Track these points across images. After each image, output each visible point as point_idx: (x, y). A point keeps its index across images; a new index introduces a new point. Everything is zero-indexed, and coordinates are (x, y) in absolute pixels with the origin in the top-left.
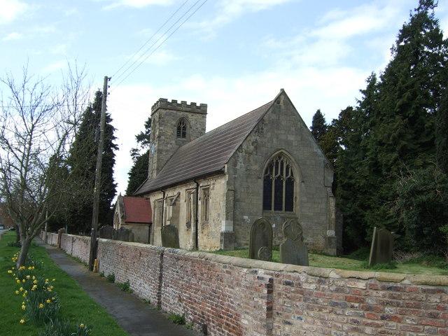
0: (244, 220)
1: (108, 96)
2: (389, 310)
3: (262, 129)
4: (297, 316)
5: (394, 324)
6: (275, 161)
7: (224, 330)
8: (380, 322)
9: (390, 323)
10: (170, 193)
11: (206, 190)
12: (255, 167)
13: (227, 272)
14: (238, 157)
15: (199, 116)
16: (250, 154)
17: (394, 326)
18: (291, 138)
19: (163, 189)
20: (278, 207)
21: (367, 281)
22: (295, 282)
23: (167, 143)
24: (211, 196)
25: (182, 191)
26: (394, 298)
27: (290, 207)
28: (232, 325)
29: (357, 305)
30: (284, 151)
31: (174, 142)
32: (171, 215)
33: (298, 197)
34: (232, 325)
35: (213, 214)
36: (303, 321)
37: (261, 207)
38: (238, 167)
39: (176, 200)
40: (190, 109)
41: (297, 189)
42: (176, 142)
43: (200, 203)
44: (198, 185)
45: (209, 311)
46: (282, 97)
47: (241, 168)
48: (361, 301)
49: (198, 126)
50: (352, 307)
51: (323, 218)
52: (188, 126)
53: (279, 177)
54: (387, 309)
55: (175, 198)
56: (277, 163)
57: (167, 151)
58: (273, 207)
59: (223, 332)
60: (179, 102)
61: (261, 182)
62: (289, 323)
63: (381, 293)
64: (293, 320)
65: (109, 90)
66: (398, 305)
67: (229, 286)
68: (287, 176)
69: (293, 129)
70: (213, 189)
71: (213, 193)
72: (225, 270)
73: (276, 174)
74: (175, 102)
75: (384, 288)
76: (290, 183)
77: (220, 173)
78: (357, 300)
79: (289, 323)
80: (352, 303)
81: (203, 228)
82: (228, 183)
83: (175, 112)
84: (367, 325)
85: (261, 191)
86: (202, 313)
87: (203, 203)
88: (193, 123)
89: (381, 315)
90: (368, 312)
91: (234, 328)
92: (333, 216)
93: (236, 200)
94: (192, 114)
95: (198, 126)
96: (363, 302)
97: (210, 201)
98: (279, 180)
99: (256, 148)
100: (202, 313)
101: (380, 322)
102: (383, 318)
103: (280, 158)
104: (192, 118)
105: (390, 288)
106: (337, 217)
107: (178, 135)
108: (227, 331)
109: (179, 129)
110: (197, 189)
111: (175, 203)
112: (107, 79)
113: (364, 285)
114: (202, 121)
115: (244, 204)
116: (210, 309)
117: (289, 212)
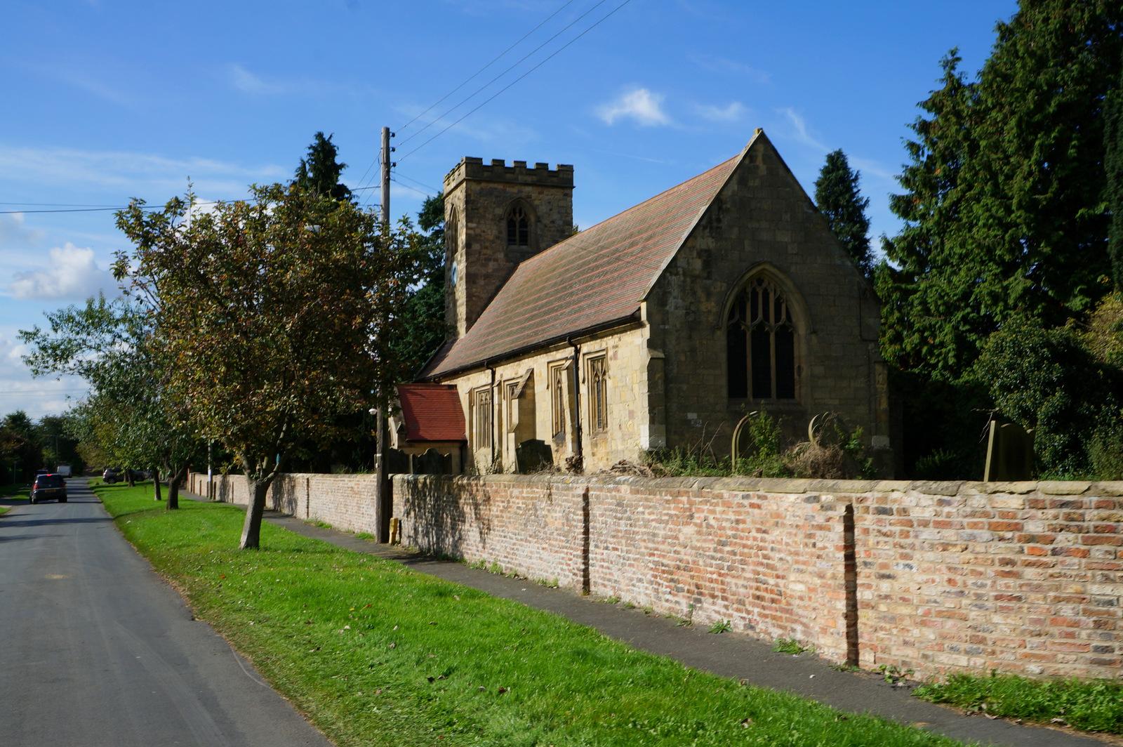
0: (688, 422)
1: (392, 169)
2: (1063, 540)
3: (719, 220)
4: (902, 562)
5: (1076, 560)
6: (749, 290)
7: (750, 608)
8: (1049, 559)
9: (1068, 560)
10: (506, 372)
11: (598, 361)
12: (708, 306)
13: (752, 505)
14: (669, 283)
15: (558, 193)
16: (695, 278)
17: (1074, 564)
18: (783, 237)
19: (492, 363)
20: (761, 391)
21: (1024, 496)
22: (895, 507)
23: (488, 260)
24: (610, 373)
25: (539, 364)
26: (1073, 520)
27: (787, 390)
28: (768, 596)
29: (1009, 535)
30: (767, 267)
31: (501, 256)
32: (515, 420)
33: (803, 365)
34: (768, 596)
35: (616, 413)
36: (914, 570)
37: (724, 392)
38: (670, 306)
39: (525, 387)
40: (535, 178)
41: (801, 349)
42: (506, 255)
43: (583, 389)
44: (577, 351)
45: (711, 581)
46: (761, 147)
47: (676, 308)
48: (1017, 527)
49: (555, 216)
50: (1001, 539)
51: (862, 410)
52: (532, 218)
53: (761, 327)
54: (1061, 537)
55: (522, 381)
56: (755, 294)
57: (487, 276)
58: (750, 392)
59: (748, 612)
60: (509, 163)
61: (721, 338)
62: (889, 577)
63: (1051, 512)
64: (898, 569)
65: (394, 157)
66: (1080, 530)
67: (759, 530)
68: (777, 319)
69: (787, 217)
70: (615, 356)
71: (613, 367)
72: (746, 502)
73: (754, 317)
74: (499, 163)
75: (1054, 505)
76: (786, 335)
77: (632, 322)
78: (1009, 527)
79: (889, 577)
80: (1001, 533)
81: (595, 445)
82: (651, 344)
83: (500, 187)
84: (1029, 564)
85: (723, 357)
86: (698, 586)
87: (591, 390)
88: (543, 209)
89: (1051, 547)
90: (1031, 545)
91: (773, 601)
92: (884, 405)
93: (667, 380)
94: (540, 189)
95: (555, 216)
96: (1018, 530)
97: (609, 383)
98: (760, 334)
99: (707, 264)
100: (698, 586)
101: (1049, 559)
102: (1055, 552)
103: (760, 282)
104: (541, 200)
105: (1064, 505)
106: (892, 405)
107: (511, 240)
108: (756, 610)
109: (511, 224)
110: (576, 359)
111: (525, 394)
112: (388, 134)
113: (1021, 502)
114: (562, 203)
115: (685, 387)
116: (715, 576)
117: (785, 401)
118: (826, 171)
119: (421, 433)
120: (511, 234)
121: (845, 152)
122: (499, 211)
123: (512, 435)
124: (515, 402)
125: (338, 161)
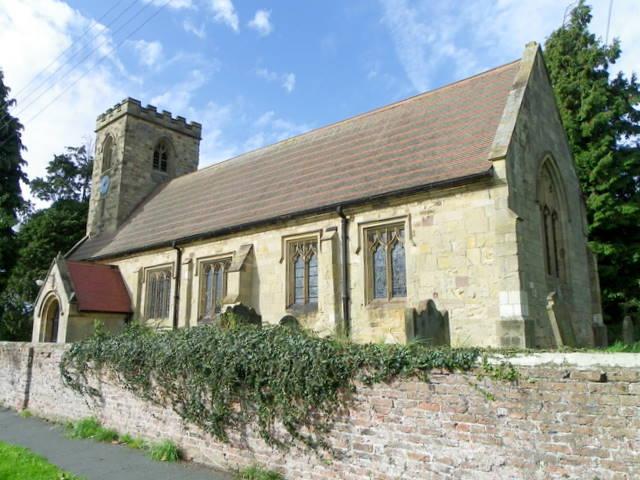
43: (144, 285)
57: (136, 188)
88: (180, 149)
104: (179, 142)
109: (156, 154)
120: (156, 161)
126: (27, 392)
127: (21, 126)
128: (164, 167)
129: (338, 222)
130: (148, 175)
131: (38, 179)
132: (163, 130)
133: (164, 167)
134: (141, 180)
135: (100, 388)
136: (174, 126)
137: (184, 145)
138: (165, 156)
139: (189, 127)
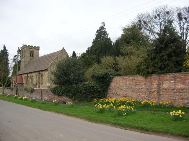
10: (30, 75)
25: (34, 74)
32: (31, 81)
43: (40, 78)
44: (39, 73)
49: (37, 53)
57: (27, 61)
71: (44, 75)
88: (35, 52)
104: (35, 51)
109: (31, 54)
110: (39, 74)
118: (73, 53)
119: (80, 56)
120: (31, 55)
121: (74, 51)
122: (29, 52)
123: (30, 84)
124: (31, 79)
125: (107, 33)
126: (41, 97)
127: (101, 33)
128: (32, 56)
129: (38, 73)
130: (29, 58)
131: (122, 34)
132: (31, 49)
133: (32, 56)
134: (28, 60)
135: (115, 59)
136: (34, 48)
137: (36, 51)
138: (32, 54)
139: (37, 48)
